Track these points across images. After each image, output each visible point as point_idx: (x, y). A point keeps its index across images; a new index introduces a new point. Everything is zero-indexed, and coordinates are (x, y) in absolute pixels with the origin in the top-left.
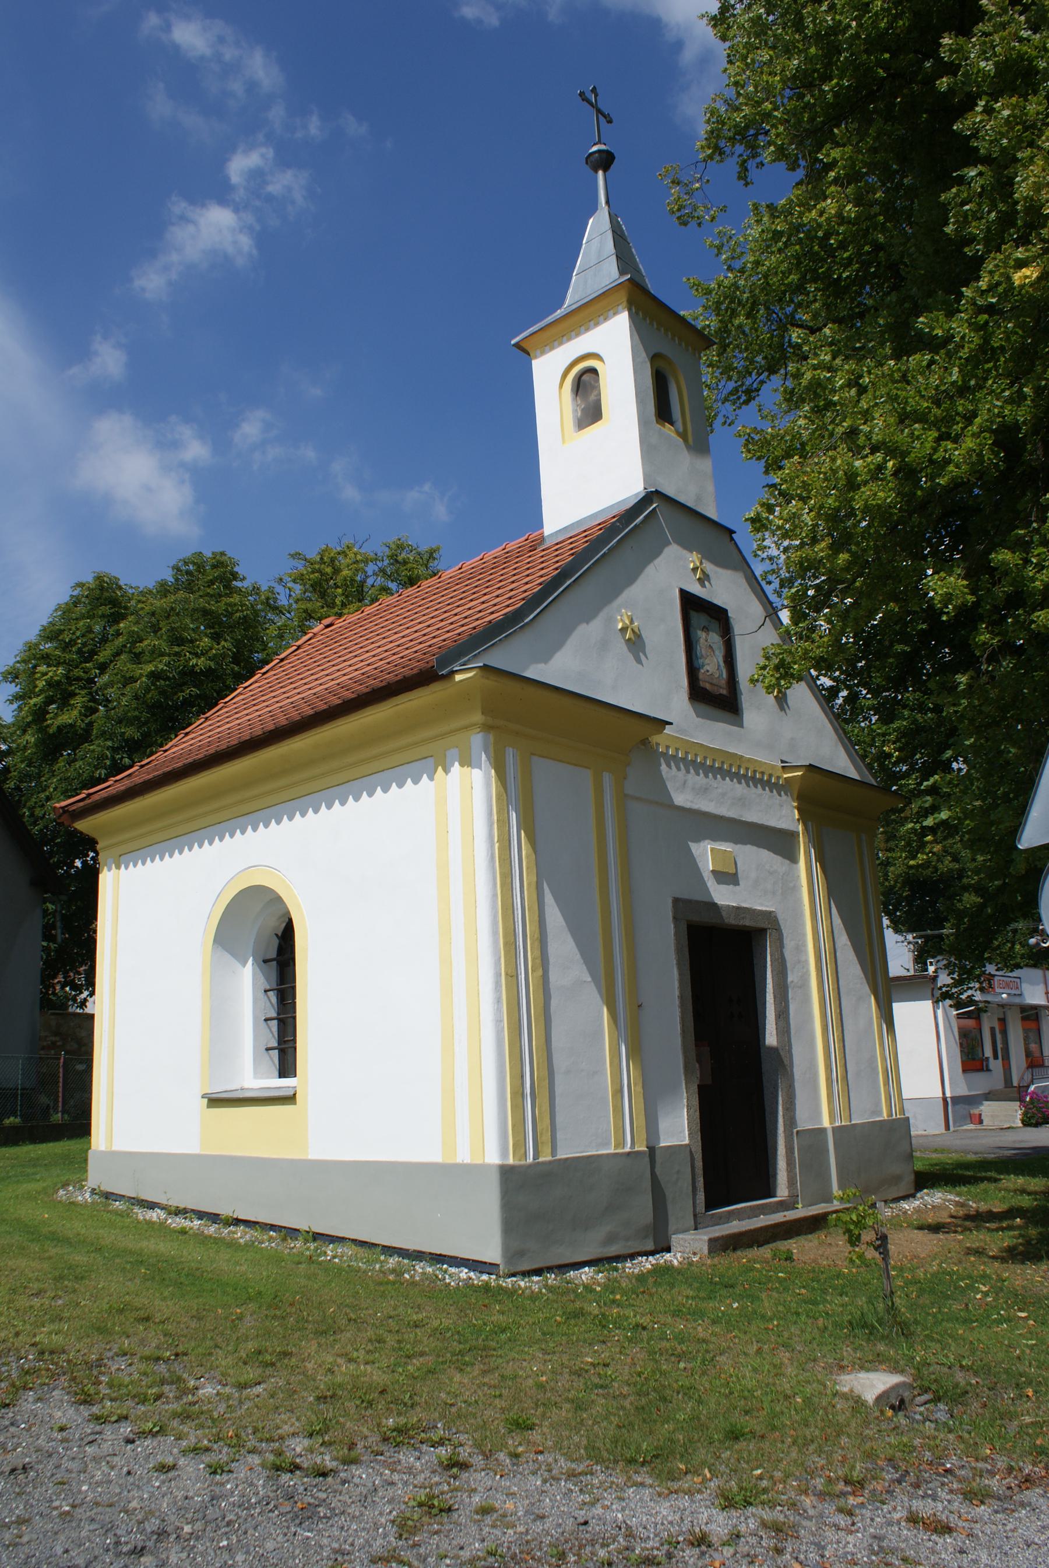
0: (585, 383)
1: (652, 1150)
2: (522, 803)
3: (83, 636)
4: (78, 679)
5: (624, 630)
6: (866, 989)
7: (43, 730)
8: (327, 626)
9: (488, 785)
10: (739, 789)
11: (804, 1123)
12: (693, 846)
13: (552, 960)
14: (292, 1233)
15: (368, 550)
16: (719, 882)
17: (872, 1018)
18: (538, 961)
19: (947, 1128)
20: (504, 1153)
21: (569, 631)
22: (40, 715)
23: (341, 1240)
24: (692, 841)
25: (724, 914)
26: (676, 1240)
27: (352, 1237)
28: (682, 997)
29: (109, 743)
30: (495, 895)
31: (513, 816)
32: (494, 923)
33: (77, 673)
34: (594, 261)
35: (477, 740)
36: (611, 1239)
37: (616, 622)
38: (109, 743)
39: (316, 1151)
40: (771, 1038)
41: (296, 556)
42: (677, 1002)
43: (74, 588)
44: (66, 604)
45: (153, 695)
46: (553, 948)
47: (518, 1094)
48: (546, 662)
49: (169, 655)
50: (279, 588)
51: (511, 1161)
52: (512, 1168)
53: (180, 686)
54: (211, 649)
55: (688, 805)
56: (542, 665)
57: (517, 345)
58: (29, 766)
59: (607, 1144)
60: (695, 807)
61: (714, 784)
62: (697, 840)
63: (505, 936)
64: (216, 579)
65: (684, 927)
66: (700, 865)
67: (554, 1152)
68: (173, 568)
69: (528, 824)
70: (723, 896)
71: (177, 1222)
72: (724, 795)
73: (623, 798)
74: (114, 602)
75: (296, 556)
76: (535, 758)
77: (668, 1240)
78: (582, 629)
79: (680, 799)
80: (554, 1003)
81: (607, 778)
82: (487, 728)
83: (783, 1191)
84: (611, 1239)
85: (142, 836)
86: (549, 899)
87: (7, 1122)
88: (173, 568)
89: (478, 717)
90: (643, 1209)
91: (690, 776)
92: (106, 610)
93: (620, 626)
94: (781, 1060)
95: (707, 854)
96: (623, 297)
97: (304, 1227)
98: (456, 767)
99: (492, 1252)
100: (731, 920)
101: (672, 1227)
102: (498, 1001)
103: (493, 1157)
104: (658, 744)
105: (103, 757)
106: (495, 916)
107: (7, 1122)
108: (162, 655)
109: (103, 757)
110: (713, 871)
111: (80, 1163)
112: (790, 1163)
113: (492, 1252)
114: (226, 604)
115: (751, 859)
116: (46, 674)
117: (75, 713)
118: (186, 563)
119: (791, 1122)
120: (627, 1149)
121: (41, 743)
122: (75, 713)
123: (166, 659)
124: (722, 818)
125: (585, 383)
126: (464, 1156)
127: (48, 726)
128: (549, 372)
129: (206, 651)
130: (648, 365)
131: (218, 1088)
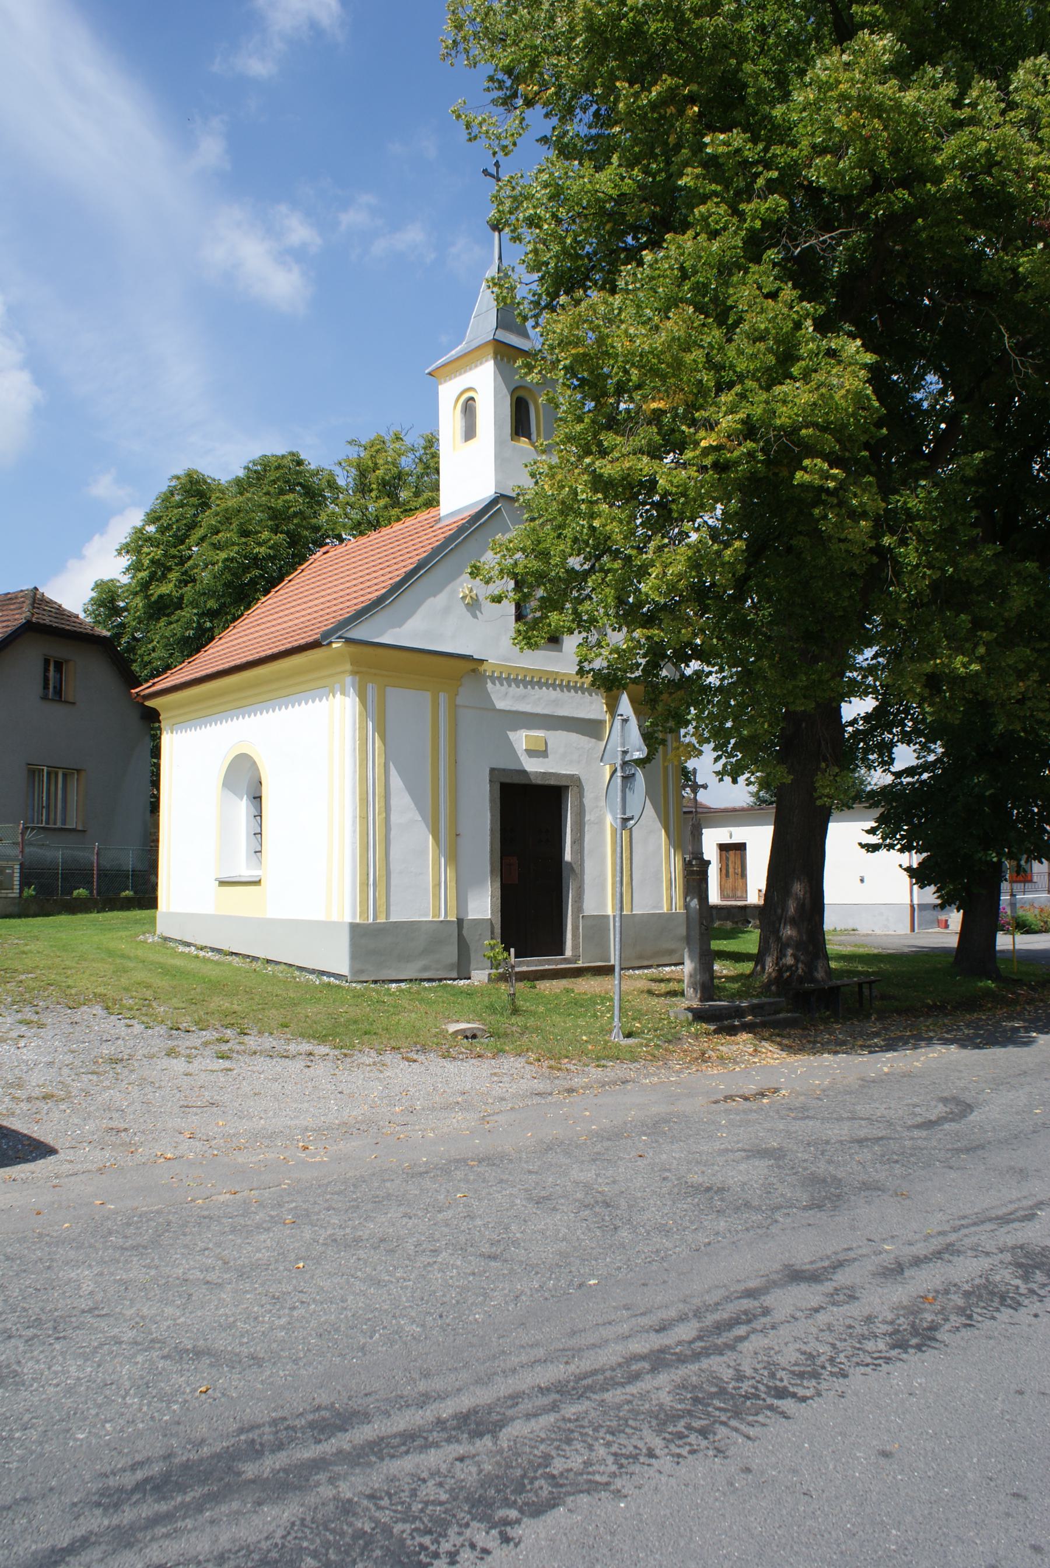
0: (469, 408)
1: (460, 922)
2: (378, 717)
3: (177, 521)
4: (174, 557)
5: (464, 598)
6: (659, 825)
7: (147, 597)
8: (325, 553)
9: (354, 707)
10: (554, 694)
11: (590, 908)
12: (512, 735)
13: (393, 808)
14: (255, 959)
15: (409, 440)
16: (530, 757)
17: (661, 845)
18: (383, 809)
19: (913, 929)
20: (354, 915)
21: (419, 604)
22: (145, 586)
23: (279, 963)
24: (511, 730)
25: (532, 777)
26: (474, 973)
27: (311, 967)
28: (492, 830)
29: (195, 611)
30: (355, 772)
31: (370, 724)
32: (354, 787)
33: (173, 551)
34: (484, 309)
35: (348, 680)
36: (425, 969)
37: (459, 593)
38: (195, 611)
39: (271, 914)
40: (568, 857)
41: (351, 442)
42: (489, 832)
43: (171, 480)
44: (165, 494)
45: (228, 576)
46: (394, 802)
47: (364, 884)
48: (400, 626)
49: (238, 544)
50: (337, 470)
51: (358, 921)
52: (358, 925)
53: (246, 569)
54: (270, 539)
55: (508, 708)
56: (398, 629)
57: (430, 374)
58: (139, 623)
59: (427, 915)
60: (514, 709)
61: (532, 692)
62: (515, 729)
63: (360, 794)
64: (278, 479)
65: (498, 787)
66: (515, 746)
67: (388, 916)
68: (245, 468)
69: (382, 729)
70: (533, 766)
71: (202, 954)
72: (539, 699)
73: (454, 709)
74: (201, 494)
75: (351, 442)
76: (388, 689)
77: (469, 973)
78: (431, 601)
79: (500, 705)
80: (393, 833)
81: (442, 697)
82: (354, 673)
83: (569, 953)
84: (425, 969)
85: (185, 714)
86: (393, 772)
87: (123, 894)
88: (245, 468)
89: (348, 667)
90: (451, 953)
91: (511, 689)
92: (194, 500)
93: (461, 595)
94: (577, 870)
95: (521, 739)
96: (490, 350)
97: (261, 955)
98: (338, 695)
99: (344, 969)
100: (539, 782)
101: (472, 966)
102: (354, 831)
103: (348, 919)
104: (485, 671)
105: (191, 621)
106: (355, 783)
107: (123, 894)
108: (233, 544)
109: (191, 621)
110: (526, 750)
111: (153, 921)
112: (575, 936)
113: (344, 969)
114: (284, 501)
115: (559, 740)
116: (149, 554)
117: (171, 585)
118: (255, 464)
119: (579, 909)
120: (442, 919)
121: (149, 606)
122: (171, 585)
123: (236, 548)
124: (537, 715)
125: (469, 408)
126: (335, 918)
127: (152, 595)
128: (449, 392)
129: (267, 541)
130: (509, 397)
131: (225, 875)
